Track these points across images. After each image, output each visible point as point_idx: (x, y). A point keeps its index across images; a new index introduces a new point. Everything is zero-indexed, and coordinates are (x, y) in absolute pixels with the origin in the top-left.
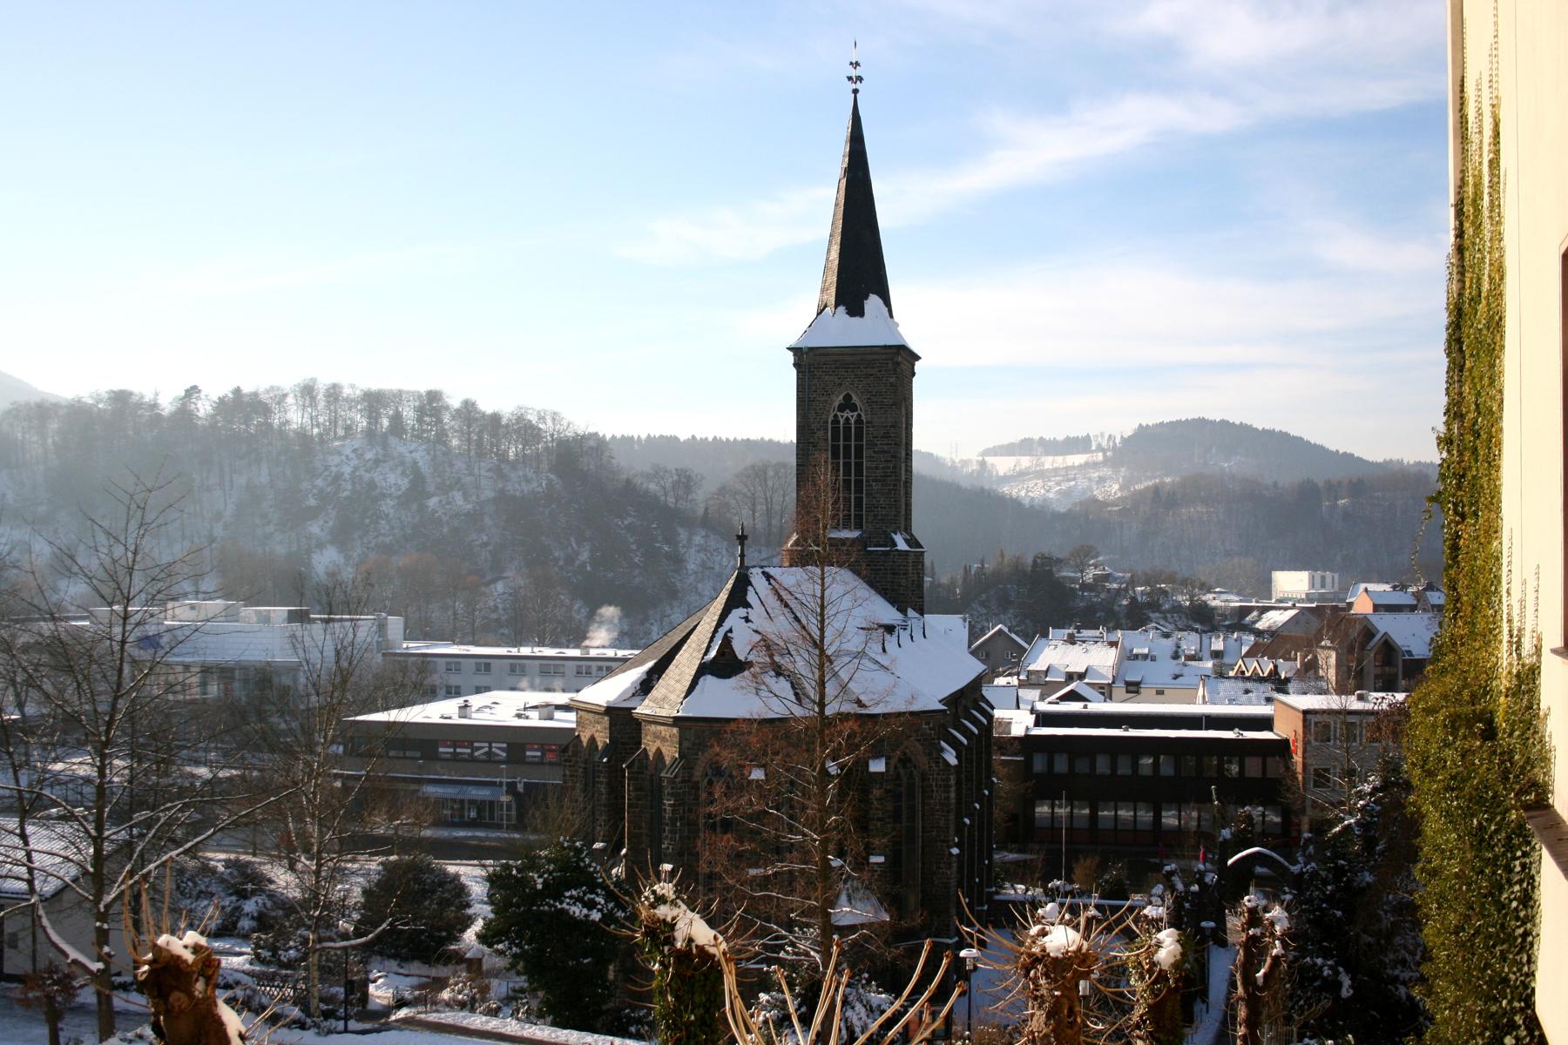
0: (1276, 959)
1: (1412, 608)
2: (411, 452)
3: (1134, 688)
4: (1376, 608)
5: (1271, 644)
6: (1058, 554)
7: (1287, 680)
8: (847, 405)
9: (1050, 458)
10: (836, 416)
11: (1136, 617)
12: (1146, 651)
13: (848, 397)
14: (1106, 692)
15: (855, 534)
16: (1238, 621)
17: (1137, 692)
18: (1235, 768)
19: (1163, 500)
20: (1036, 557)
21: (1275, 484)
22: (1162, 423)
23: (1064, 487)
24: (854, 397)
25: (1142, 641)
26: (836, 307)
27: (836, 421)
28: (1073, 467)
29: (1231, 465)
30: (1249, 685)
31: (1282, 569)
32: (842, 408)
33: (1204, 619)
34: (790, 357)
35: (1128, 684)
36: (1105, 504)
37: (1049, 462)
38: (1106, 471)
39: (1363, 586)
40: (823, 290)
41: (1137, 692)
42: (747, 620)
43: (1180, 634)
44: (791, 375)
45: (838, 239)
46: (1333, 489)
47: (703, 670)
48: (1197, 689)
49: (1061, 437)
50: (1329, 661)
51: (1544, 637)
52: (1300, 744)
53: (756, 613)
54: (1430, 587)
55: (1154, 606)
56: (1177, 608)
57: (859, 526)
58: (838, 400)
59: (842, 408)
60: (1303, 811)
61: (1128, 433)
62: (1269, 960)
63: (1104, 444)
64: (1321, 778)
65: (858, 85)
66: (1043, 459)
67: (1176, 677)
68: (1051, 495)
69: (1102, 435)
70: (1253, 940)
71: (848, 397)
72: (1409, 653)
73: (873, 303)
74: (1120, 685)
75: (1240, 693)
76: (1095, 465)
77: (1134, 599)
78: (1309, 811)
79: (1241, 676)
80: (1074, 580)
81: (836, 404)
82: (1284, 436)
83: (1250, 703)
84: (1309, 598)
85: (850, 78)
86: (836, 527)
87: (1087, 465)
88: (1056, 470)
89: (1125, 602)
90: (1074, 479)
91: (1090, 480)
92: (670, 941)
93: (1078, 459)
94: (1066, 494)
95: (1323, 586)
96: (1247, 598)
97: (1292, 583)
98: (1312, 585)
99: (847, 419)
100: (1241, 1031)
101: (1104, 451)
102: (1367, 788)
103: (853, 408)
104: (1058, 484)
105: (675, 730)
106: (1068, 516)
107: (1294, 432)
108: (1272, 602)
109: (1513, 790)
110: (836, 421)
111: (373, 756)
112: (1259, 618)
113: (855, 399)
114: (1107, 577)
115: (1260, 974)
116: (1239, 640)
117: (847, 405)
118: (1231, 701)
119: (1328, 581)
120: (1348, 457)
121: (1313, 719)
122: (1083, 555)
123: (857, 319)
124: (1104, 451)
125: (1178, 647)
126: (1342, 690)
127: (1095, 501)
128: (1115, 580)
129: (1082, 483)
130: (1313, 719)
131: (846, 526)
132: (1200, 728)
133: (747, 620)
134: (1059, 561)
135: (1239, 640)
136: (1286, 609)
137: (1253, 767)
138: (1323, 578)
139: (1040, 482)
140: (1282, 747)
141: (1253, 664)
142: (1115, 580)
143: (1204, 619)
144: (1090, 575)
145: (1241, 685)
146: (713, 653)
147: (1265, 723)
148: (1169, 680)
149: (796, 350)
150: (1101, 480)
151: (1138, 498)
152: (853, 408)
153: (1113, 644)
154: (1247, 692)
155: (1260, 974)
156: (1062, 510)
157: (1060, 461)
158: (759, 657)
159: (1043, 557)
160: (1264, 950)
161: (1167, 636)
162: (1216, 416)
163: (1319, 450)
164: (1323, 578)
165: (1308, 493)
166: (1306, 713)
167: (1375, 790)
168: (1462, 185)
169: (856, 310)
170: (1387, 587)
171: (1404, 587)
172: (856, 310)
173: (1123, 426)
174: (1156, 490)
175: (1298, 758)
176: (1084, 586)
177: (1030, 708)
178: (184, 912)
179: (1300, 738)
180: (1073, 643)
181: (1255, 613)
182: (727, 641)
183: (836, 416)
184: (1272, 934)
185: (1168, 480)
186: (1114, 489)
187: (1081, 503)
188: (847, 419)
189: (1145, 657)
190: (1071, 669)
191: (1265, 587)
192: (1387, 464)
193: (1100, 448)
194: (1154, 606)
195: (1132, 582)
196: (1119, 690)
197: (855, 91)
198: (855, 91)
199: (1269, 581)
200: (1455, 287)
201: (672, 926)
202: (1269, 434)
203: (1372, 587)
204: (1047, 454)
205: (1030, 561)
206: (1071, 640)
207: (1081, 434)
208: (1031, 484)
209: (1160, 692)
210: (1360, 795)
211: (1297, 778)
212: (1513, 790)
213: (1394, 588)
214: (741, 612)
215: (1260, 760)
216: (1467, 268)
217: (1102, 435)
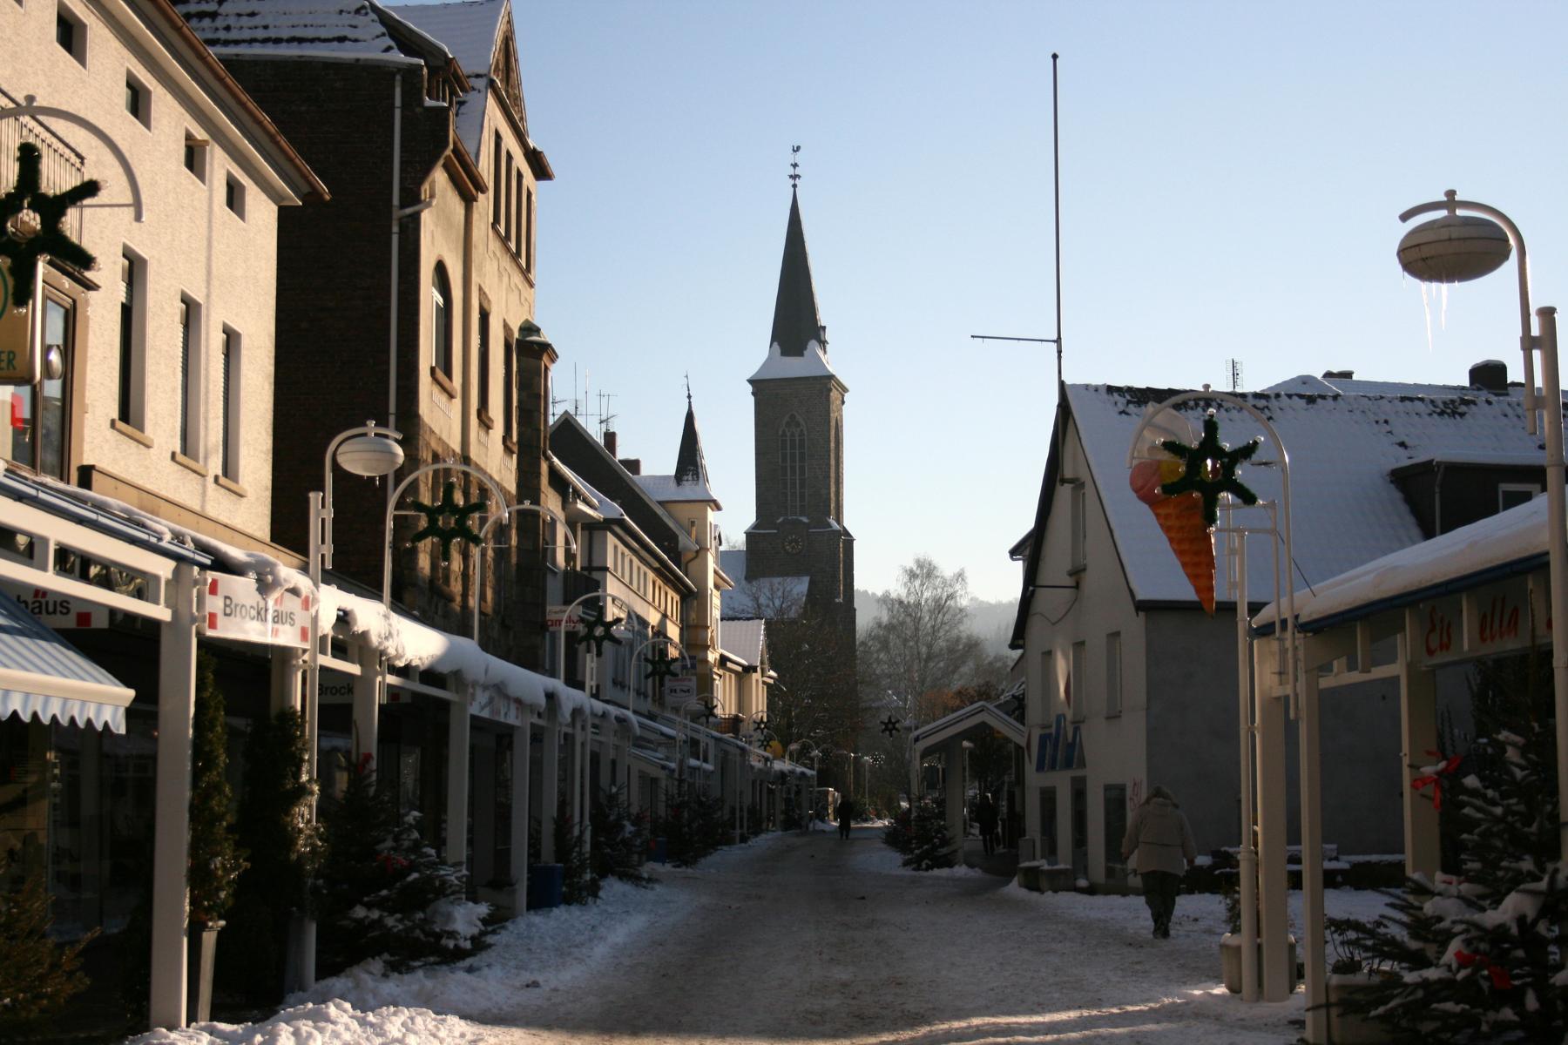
10: (784, 431)
18: (54, 785)
24: (798, 417)
27: (784, 434)
34: (750, 388)
44: (749, 402)
51: (406, 649)
59: (788, 424)
85: (791, 177)
109: (416, 847)
110: (784, 434)
149: (750, 381)
152: (798, 425)
177: (1282, 671)
178: (693, 762)
183: (784, 431)
197: (795, 186)
198: (795, 186)
211: (783, 776)
212: (416, 847)
216: (93, 164)
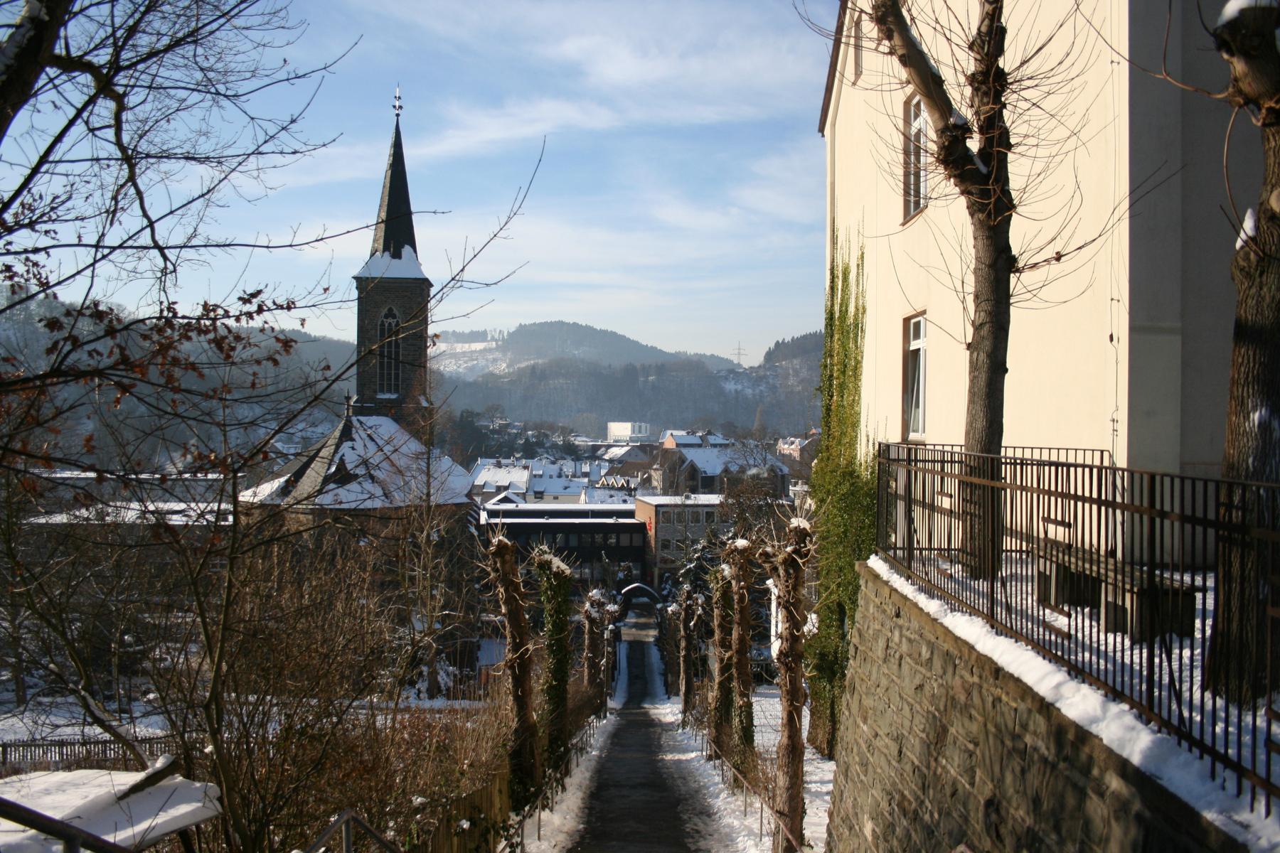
0: (699, 616)
1: (700, 446)
2: (5, 330)
3: (539, 496)
4: (678, 445)
5: (620, 466)
6: (477, 409)
7: (635, 489)
8: (390, 314)
9: (460, 345)
11: (530, 451)
12: (541, 472)
13: (390, 310)
14: (524, 496)
15: (394, 396)
16: (593, 454)
17: (542, 498)
18: (613, 541)
19: (536, 374)
20: (463, 412)
21: (610, 366)
22: (534, 324)
23: (470, 364)
25: (541, 466)
26: (384, 251)
28: (475, 351)
29: (580, 353)
30: (612, 492)
31: (614, 421)
32: (386, 316)
33: (572, 452)
34: (354, 284)
35: (536, 493)
36: (501, 377)
37: (460, 348)
38: (498, 355)
39: (669, 432)
40: (375, 241)
41: (542, 498)
42: (353, 448)
43: (562, 462)
45: (385, 208)
46: (646, 370)
47: (327, 480)
48: (580, 496)
49: (467, 331)
50: (657, 478)
52: (653, 525)
53: (359, 444)
54: (709, 433)
55: (540, 444)
56: (555, 446)
57: (397, 391)
58: (384, 311)
59: (386, 316)
60: (655, 564)
61: (512, 329)
62: (695, 618)
63: (496, 336)
64: (665, 545)
65: (399, 112)
66: (456, 345)
67: (566, 488)
68: (461, 370)
69: (495, 330)
70: (689, 607)
71: (390, 310)
72: (705, 472)
73: (407, 250)
74: (531, 494)
75: (607, 497)
76: (490, 350)
77: (527, 440)
78: (659, 565)
79: (604, 487)
80: (487, 427)
81: (383, 314)
82: (614, 334)
83: (613, 503)
84: (632, 440)
85: (394, 107)
86: (382, 391)
87: (485, 350)
88: (464, 353)
89: (522, 442)
90: (477, 359)
91: (487, 360)
92: (550, 568)
93: (478, 346)
94: (472, 369)
95: (640, 432)
96: (596, 439)
97: (620, 430)
98: (633, 432)
99: (390, 324)
100: (683, 653)
101: (496, 341)
102: (700, 547)
103: (394, 317)
104: (465, 362)
105: (310, 517)
106: (473, 385)
107: (620, 332)
108: (610, 441)
111: (10, 548)
112: (606, 452)
113: (395, 311)
114: (507, 426)
115: (692, 623)
116: (599, 465)
117: (390, 314)
118: (602, 502)
119: (643, 428)
120: (653, 349)
121: (662, 510)
122: (494, 410)
123: (396, 261)
124: (496, 341)
125: (561, 470)
126: (665, 493)
127: (492, 374)
128: (514, 427)
129: (482, 363)
130: (662, 510)
131: (389, 391)
132: (587, 517)
133: (353, 448)
134: (478, 414)
135: (599, 465)
136: (622, 446)
137: (625, 540)
138: (640, 427)
139: (453, 361)
140: (642, 527)
141: (611, 480)
142: (514, 427)
143: (572, 452)
144: (498, 423)
145: (607, 492)
146: (333, 469)
147: (630, 514)
148: (562, 490)
150: (495, 360)
151: (521, 372)
152: (394, 317)
153: (526, 467)
154: (611, 496)
155: (692, 623)
156: (471, 380)
157: (466, 347)
158: (361, 471)
159: (468, 412)
160: (693, 613)
161: (553, 463)
162: (570, 320)
163: (636, 344)
164: (640, 427)
165: (631, 373)
166: (657, 506)
167: (704, 548)
168: (833, 261)
169: (397, 255)
170: (683, 433)
171: (694, 433)
172: (397, 255)
173: (509, 324)
174: (533, 369)
175: (652, 533)
176: (494, 431)
179: (653, 521)
180: (500, 467)
181: (603, 449)
182: (342, 460)
184: (697, 604)
185: (540, 361)
186: (502, 368)
187: (483, 376)
188: (390, 324)
189: (541, 476)
190: (499, 484)
191: (603, 433)
192: (677, 355)
193: (493, 339)
194: (540, 444)
195: (525, 429)
196: (531, 496)
197: (398, 115)
198: (398, 115)
199: (606, 428)
200: (829, 303)
201: (551, 562)
202: (604, 333)
203: (676, 433)
204: (458, 342)
205: (458, 414)
206: (499, 465)
207: (481, 329)
208: (447, 362)
209: (556, 498)
210: (696, 551)
213: (688, 433)
214: (350, 444)
215: (629, 535)
217: (495, 330)
